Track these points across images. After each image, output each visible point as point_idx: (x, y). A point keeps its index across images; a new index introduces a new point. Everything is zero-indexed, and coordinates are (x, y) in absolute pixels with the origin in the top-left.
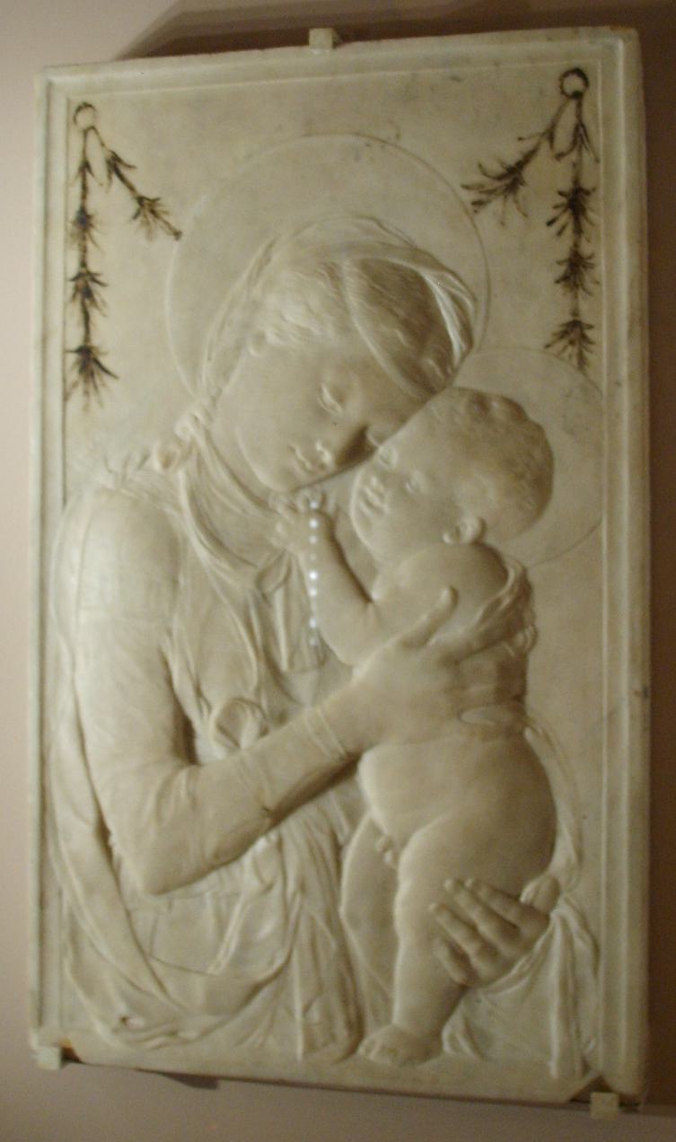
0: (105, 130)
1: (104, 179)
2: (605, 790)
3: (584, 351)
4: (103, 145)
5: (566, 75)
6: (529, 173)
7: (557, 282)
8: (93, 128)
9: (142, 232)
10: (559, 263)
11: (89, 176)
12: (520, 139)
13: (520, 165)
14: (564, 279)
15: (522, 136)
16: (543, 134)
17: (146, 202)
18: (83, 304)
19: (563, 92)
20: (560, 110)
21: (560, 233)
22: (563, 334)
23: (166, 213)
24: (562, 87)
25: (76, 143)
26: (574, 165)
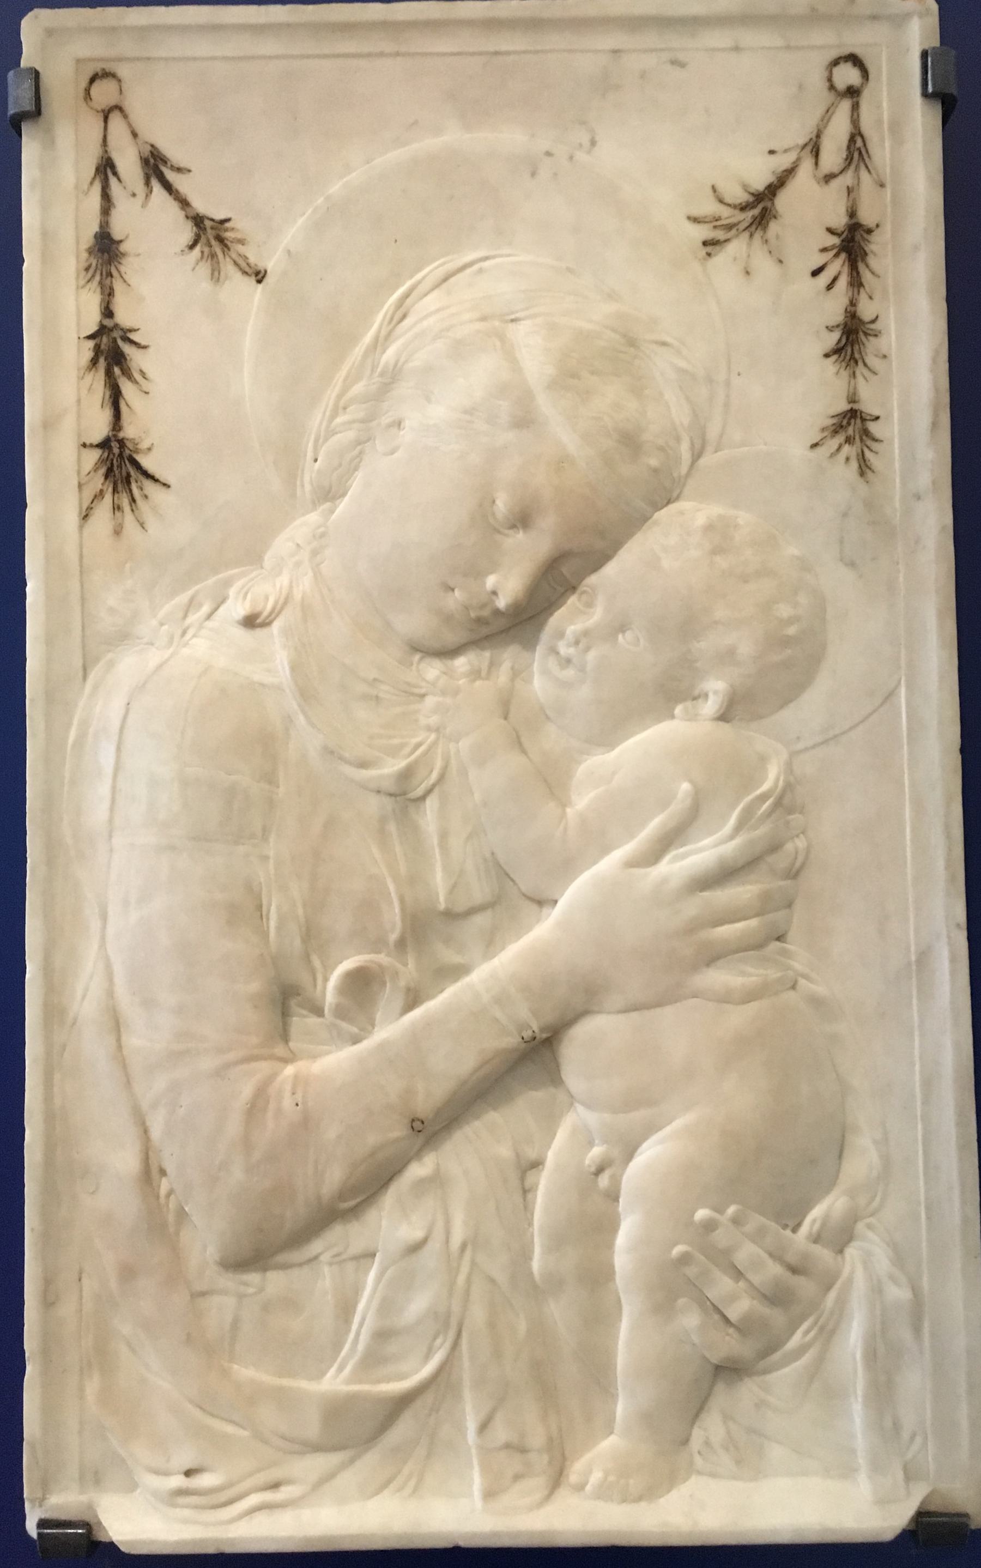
0: (136, 104)
1: (140, 188)
2: (917, 1068)
3: (867, 452)
4: (135, 135)
5: (836, 63)
6: (783, 201)
7: (827, 356)
8: (119, 108)
9: (204, 269)
10: (830, 329)
11: (113, 181)
12: (772, 152)
13: (773, 190)
14: (837, 351)
15: (772, 148)
16: (805, 145)
17: (208, 223)
18: (109, 373)
19: (832, 87)
20: (828, 113)
21: (830, 287)
22: (837, 429)
23: (242, 242)
24: (830, 79)
25: (93, 127)
26: (849, 190)
